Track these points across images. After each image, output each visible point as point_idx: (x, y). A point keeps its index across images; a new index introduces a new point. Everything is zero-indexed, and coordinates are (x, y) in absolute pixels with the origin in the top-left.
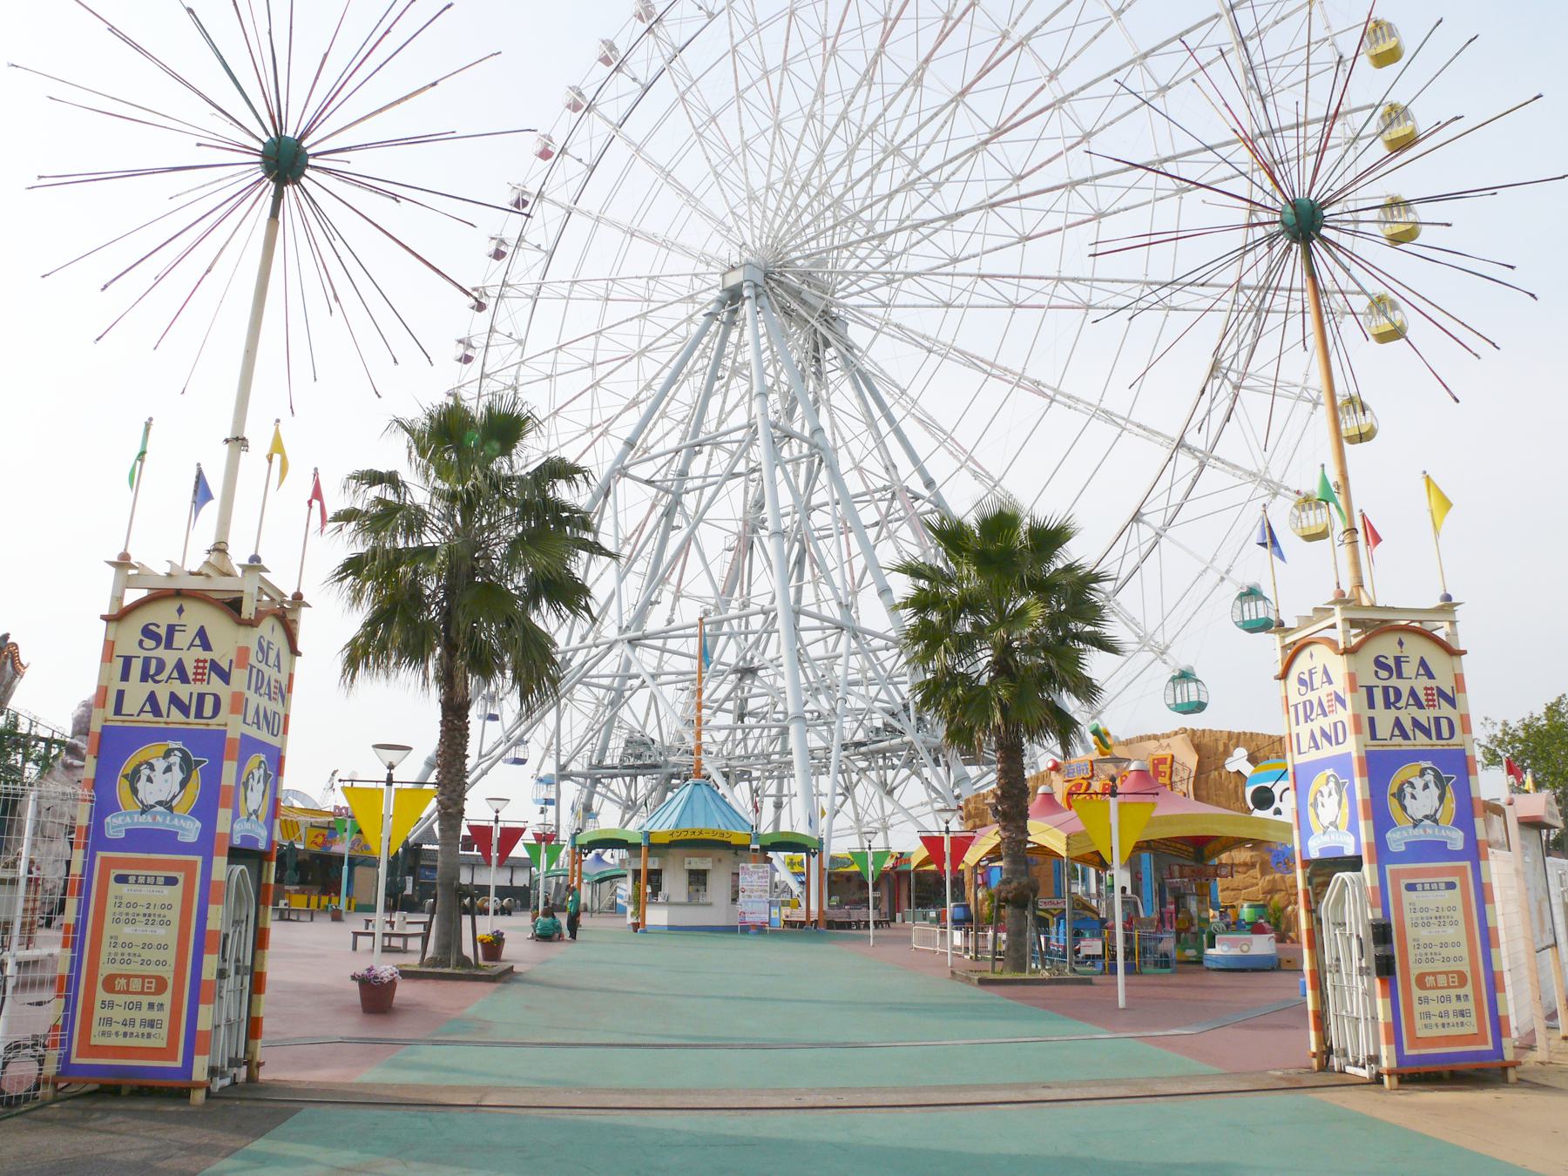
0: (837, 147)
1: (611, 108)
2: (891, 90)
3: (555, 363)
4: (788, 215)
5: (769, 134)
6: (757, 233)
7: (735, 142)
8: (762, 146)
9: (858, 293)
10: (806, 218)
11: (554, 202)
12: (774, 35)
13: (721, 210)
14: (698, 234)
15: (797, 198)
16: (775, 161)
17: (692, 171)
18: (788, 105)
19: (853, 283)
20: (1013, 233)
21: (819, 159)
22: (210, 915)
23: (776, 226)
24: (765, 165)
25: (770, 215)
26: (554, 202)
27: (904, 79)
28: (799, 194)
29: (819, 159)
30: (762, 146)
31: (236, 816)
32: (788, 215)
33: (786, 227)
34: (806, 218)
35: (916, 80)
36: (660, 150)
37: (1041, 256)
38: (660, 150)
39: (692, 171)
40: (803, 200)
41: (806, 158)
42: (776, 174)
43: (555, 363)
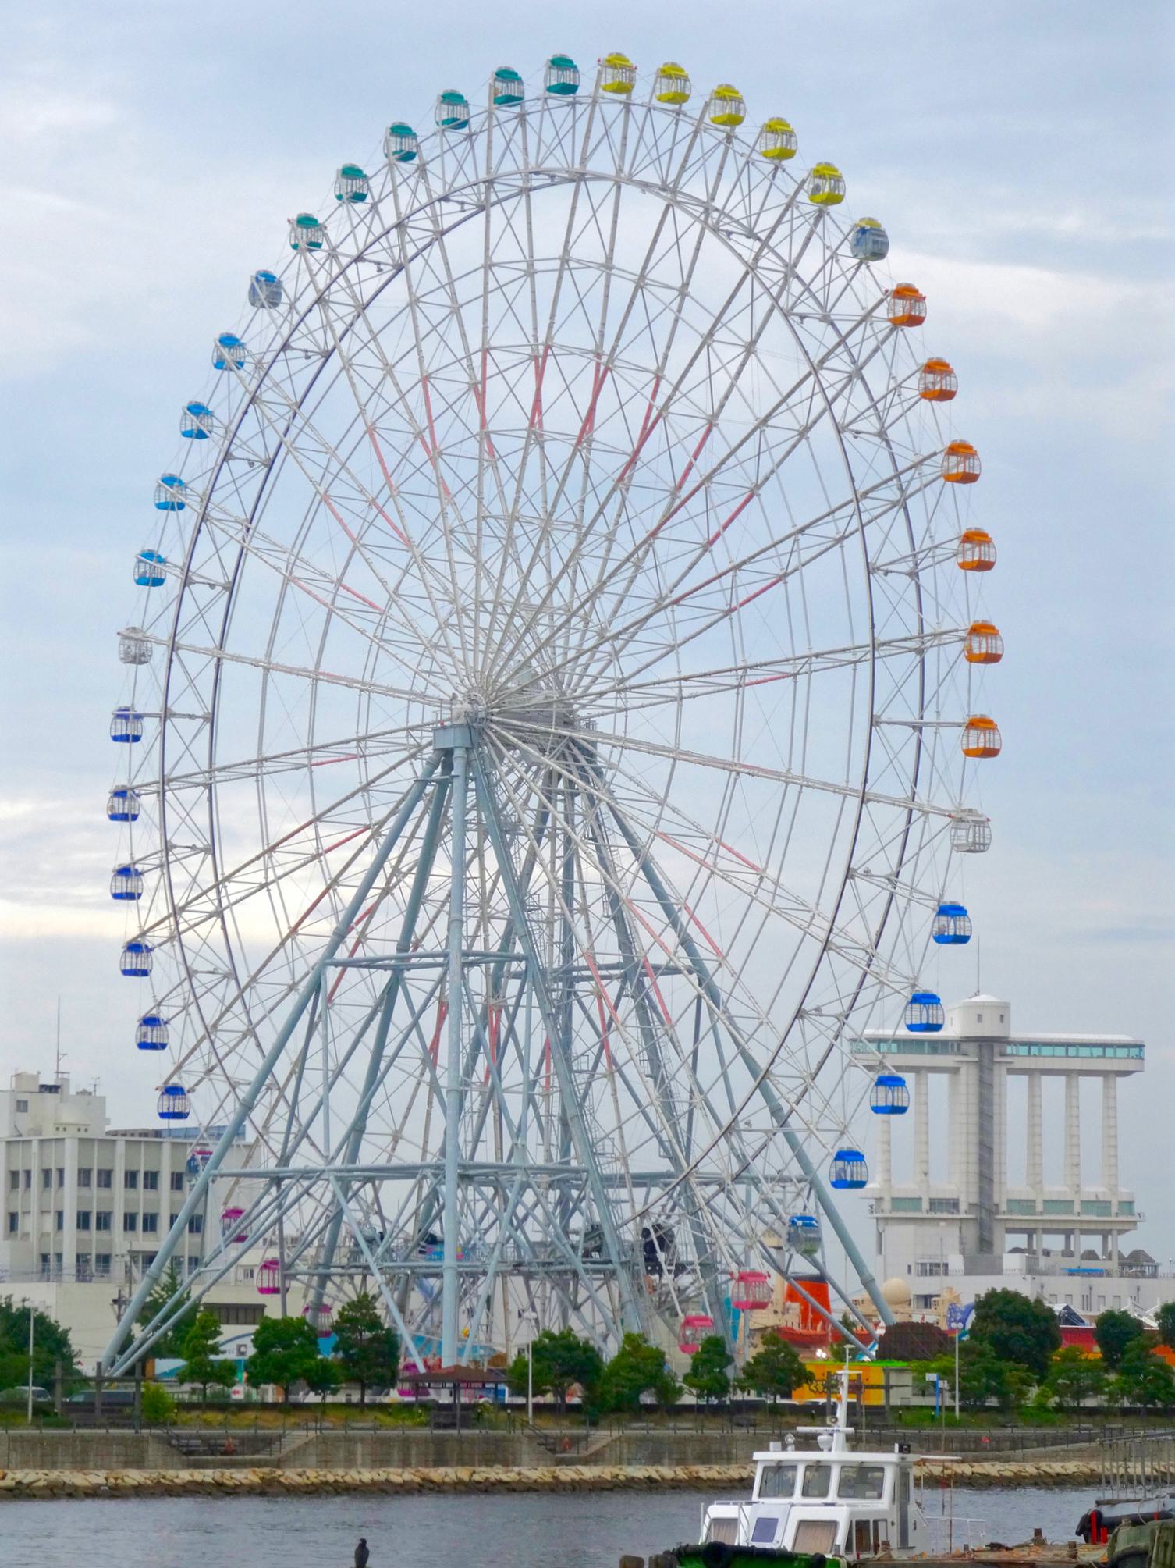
0: (491, 548)
1: (232, 503)
2: (514, 462)
3: (318, 838)
4: (476, 644)
5: (414, 570)
6: (456, 680)
7: (381, 599)
8: (411, 586)
9: (593, 682)
10: (497, 637)
11: (191, 717)
12: (363, 463)
13: (402, 680)
14: (389, 714)
15: (476, 621)
16: (436, 595)
17: (347, 653)
18: (416, 528)
19: (581, 677)
20: (694, 546)
21: (480, 565)
22: (752, 1054)
23: (471, 663)
24: (426, 605)
25: (459, 654)
26: (191, 717)
27: (522, 443)
28: (477, 616)
29: (480, 565)
30: (411, 586)
31: (479, 823)
32: (476, 644)
33: (481, 656)
34: (497, 637)
35: (535, 433)
36: (295, 652)
37: (691, 660)
38: (295, 652)
39: (347, 653)
40: (485, 620)
41: (465, 577)
42: (444, 609)
43: (318, 838)
